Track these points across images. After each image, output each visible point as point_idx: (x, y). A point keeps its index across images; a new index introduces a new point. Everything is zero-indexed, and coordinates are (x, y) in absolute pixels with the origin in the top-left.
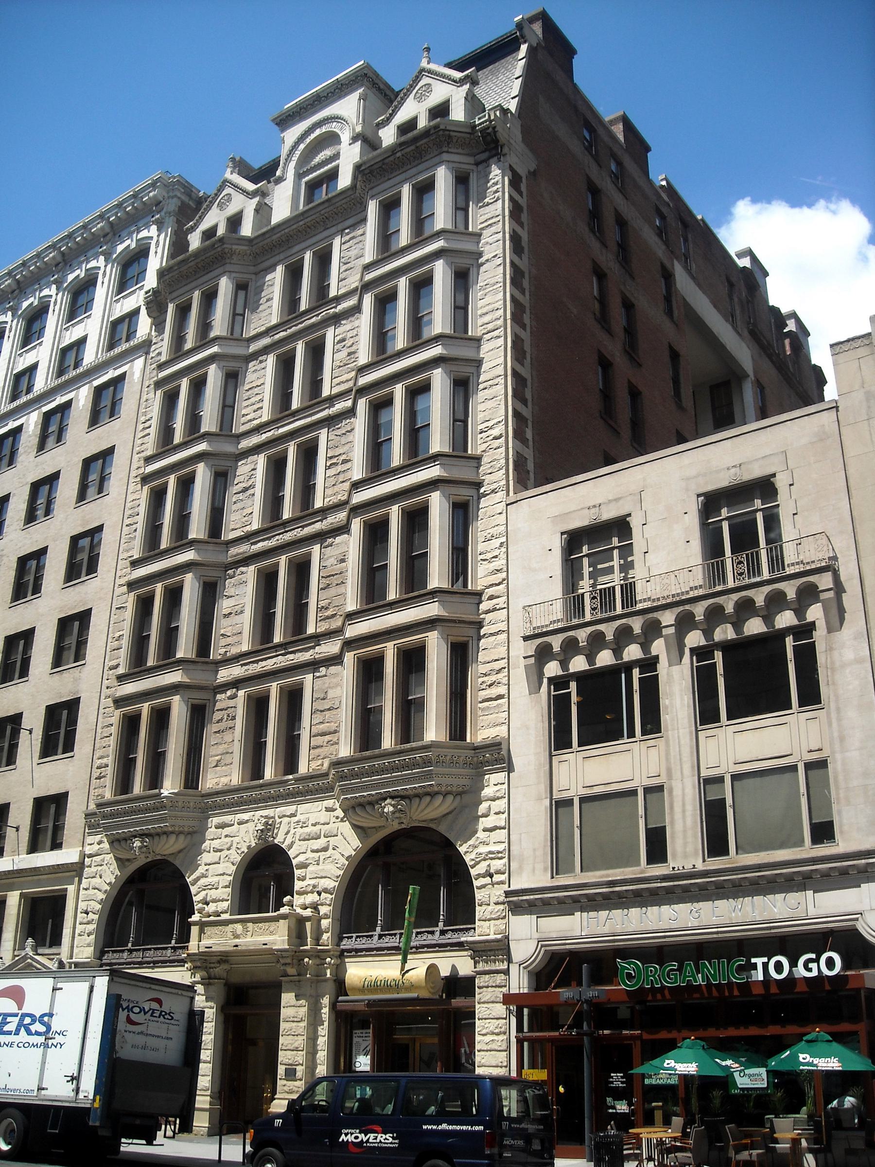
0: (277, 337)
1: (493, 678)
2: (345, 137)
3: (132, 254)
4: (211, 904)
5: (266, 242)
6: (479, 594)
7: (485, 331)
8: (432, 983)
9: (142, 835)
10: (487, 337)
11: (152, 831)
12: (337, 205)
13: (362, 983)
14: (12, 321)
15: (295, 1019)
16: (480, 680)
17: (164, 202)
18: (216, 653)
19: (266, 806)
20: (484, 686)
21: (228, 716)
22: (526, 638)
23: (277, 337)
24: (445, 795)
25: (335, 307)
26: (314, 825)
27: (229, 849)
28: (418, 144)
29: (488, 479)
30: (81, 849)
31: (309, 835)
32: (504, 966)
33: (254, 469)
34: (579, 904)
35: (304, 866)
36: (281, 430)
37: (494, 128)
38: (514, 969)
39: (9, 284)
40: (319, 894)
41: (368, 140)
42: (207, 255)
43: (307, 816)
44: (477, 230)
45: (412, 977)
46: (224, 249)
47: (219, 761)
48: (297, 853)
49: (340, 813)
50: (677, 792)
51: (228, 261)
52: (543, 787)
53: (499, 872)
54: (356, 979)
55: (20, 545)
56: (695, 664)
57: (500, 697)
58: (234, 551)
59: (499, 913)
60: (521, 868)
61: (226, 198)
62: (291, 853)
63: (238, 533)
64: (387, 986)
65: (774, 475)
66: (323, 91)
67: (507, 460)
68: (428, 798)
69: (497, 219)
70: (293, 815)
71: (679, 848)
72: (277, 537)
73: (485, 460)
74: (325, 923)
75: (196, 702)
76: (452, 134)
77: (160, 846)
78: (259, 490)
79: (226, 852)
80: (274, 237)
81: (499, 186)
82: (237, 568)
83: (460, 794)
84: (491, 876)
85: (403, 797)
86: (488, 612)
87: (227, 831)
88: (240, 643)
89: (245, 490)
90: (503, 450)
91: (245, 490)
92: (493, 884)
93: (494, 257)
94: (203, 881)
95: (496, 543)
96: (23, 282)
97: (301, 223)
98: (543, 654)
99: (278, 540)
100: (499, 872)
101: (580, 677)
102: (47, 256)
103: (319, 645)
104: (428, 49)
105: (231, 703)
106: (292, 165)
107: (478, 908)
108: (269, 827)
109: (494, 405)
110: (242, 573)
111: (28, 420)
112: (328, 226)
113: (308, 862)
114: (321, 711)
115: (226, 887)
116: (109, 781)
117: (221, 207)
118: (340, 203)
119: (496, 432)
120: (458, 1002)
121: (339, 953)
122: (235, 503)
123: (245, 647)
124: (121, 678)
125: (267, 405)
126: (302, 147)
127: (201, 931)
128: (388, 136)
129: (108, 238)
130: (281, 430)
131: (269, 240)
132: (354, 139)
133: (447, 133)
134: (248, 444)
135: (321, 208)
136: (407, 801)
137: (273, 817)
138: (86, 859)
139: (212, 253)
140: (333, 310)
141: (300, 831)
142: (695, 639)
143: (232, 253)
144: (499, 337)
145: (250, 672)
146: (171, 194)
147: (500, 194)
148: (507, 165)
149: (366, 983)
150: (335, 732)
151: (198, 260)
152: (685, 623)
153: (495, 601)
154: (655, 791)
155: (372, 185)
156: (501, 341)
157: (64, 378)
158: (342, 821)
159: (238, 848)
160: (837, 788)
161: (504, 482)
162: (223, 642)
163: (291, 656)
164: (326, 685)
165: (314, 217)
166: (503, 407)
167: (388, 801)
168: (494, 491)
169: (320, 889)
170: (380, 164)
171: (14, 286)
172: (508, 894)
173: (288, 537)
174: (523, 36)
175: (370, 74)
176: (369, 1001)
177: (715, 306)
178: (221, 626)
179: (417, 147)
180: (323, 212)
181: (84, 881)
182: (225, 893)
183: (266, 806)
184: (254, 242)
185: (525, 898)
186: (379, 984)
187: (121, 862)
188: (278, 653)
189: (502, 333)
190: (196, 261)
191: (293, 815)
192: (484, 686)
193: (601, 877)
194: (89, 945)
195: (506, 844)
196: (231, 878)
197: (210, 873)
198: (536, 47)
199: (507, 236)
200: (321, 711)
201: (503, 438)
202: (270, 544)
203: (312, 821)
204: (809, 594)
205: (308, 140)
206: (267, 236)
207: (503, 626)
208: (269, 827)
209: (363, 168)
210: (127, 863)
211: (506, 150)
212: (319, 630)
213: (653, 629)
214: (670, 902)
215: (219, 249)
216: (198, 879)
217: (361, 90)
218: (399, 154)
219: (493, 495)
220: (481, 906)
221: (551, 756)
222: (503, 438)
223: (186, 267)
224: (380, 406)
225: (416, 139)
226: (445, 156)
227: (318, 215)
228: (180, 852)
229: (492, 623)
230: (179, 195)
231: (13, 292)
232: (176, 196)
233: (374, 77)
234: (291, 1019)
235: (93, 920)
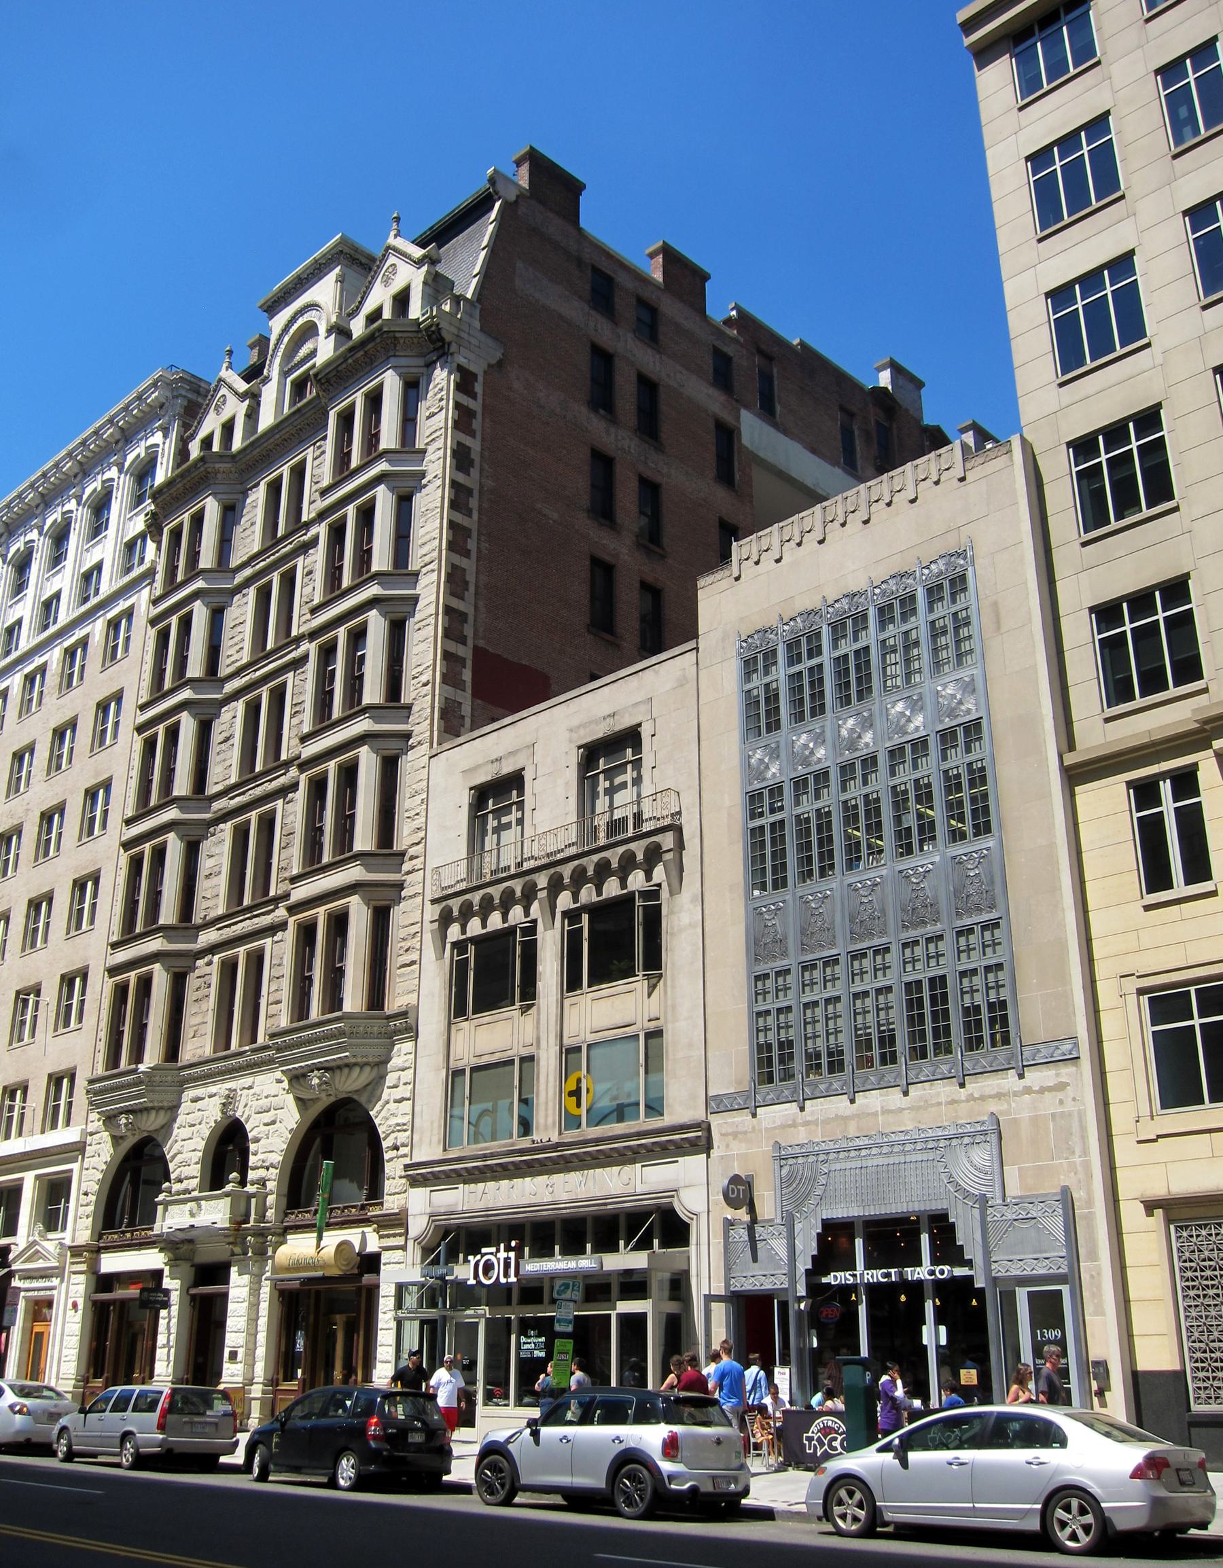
0: (258, 567)
2: (322, 329)
3: (144, 463)
6: (402, 854)
7: (422, 564)
8: (346, 1260)
9: (128, 1111)
10: (424, 570)
11: (135, 1107)
12: (307, 416)
14: (164, 443)
16: (399, 945)
17: (167, 404)
18: (197, 919)
22: (434, 901)
23: (258, 567)
25: (305, 534)
26: (266, 1097)
27: (200, 1124)
29: (417, 729)
30: (84, 1127)
32: (400, 1241)
33: (235, 717)
34: (462, 1178)
35: (257, 1140)
36: (258, 673)
37: (438, 325)
38: (410, 1244)
39: (156, 397)
41: (340, 331)
44: (422, 447)
48: (253, 1127)
49: (286, 1084)
50: (543, 1063)
52: (441, 1059)
53: (404, 1145)
55: (42, 798)
56: (566, 928)
57: (413, 963)
58: (218, 805)
61: (222, 400)
62: (248, 1127)
63: (219, 788)
65: (640, 725)
66: (303, 272)
67: (433, 708)
69: (438, 433)
70: (250, 1088)
71: (542, 1121)
72: (250, 792)
73: (415, 709)
74: (271, 1199)
75: (177, 970)
76: (398, 335)
77: (143, 1123)
78: (237, 741)
79: (198, 1127)
80: (255, 452)
81: (444, 393)
85: (327, 1069)
86: (409, 873)
87: (199, 1104)
88: (216, 906)
89: (227, 740)
90: (429, 697)
91: (227, 740)
93: (435, 477)
95: (418, 799)
96: (128, 429)
97: (277, 436)
98: (445, 919)
100: (404, 1145)
101: (475, 940)
102: (149, 396)
104: (398, 219)
105: (207, 970)
106: (277, 361)
107: (386, 1182)
108: (229, 1101)
109: (425, 648)
110: (222, 831)
111: (51, 657)
112: (304, 437)
113: (260, 1136)
114: (278, 978)
115: (197, 1163)
116: (101, 1058)
117: (386, 282)
118: (309, 414)
119: (424, 678)
120: (367, 1278)
121: (281, 1231)
122: (218, 754)
123: (221, 911)
124: (115, 946)
125: (247, 645)
126: (286, 339)
127: (166, 1210)
128: (358, 327)
129: (120, 445)
132: (329, 331)
133: (391, 334)
135: (293, 419)
136: (330, 1072)
137: (235, 1090)
138: (89, 1137)
141: (255, 1103)
142: (565, 900)
143: (217, 472)
144: (433, 571)
145: (224, 937)
146: (175, 394)
147: (443, 403)
148: (455, 365)
152: (556, 886)
153: (414, 862)
154: (528, 1060)
155: (331, 395)
156: (434, 576)
157: (88, 605)
158: (288, 1093)
160: (667, 1059)
161: (428, 733)
162: (205, 904)
163: (256, 920)
165: (287, 429)
166: (432, 649)
168: (420, 743)
169: (267, 1164)
170: (334, 373)
171: (118, 436)
172: (407, 1167)
173: (258, 792)
174: (497, 193)
175: (346, 250)
176: (304, 1278)
177: (814, 451)
178: (204, 887)
179: (366, 352)
180: (295, 424)
181: (86, 1160)
182: (195, 1170)
185: (419, 1172)
187: (116, 1140)
189: (436, 567)
191: (250, 1088)
195: (410, 1117)
196: (201, 1154)
197: (185, 1149)
198: (516, 202)
199: (449, 451)
200: (278, 978)
201: (430, 685)
204: (654, 855)
205: (292, 331)
206: (248, 451)
207: (419, 889)
208: (229, 1101)
210: (120, 1141)
211: (453, 348)
212: (279, 892)
213: (529, 895)
214: (532, 1175)
215: (202, 469)
216: (175, 1155)
217: (337, 270)
218: (350, 361)
219: (419, 748)
221: (450, 1024)
222: (430, 685)
223: (175, 489)
224: (328, 652)
225: (188, 470)
226: (393, 361)
228: (163, 1127)
229: (413, 884)
230: (184, 393)
231: (117, 442)
232: (180, 395)
233: (352, 252)
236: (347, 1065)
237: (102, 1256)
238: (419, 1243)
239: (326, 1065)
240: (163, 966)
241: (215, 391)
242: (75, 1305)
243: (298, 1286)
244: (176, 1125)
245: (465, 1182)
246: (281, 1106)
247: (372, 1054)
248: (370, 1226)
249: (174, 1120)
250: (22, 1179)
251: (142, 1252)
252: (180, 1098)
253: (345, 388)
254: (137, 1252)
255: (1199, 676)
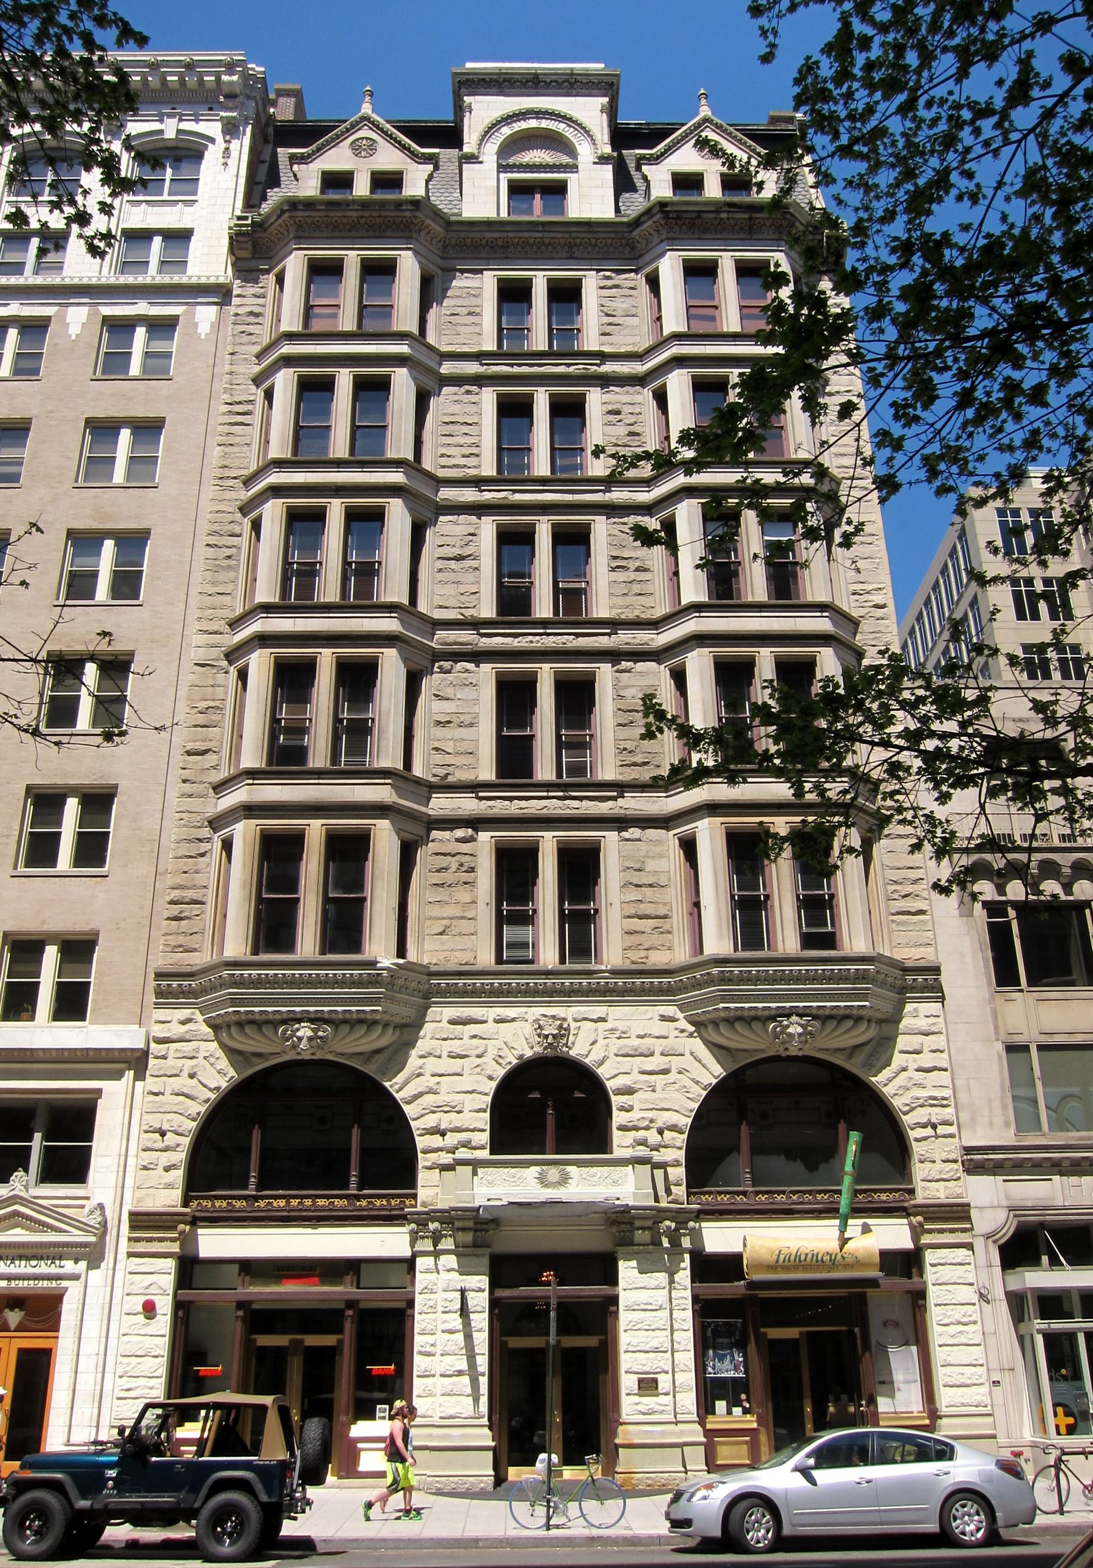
1: (910, 889)
4: (449, 1134)
5: (473, 235)
9: (316, 1020)
13: (775, 1257)
15: (650, 1307)
19: (550, 1002)
20: (896, 896)
21: (462, 865)
24: (386, 1025)
25: (598, 365)
28: (755, 215)
31: (636, 1050)
36: (518, 497)
40: (661, 1132)
42: (383, 213)
43: (628, 1023)
45: (857, 1250)
46: (415, 217)
47: (447, 927)
51: (415, 236)
54: (764, 1251)
59: (952, 1174)
60: (973, 1120)
64: (816, 1262)
68: (347, 1028)
72: (530, 638)
80: (488, 235)
82: (456, 662)
83: (880, 1022)
84: (163, 1134)
85: (815, 1017)
92: (937, 1137)
94: (428, 1100)
99: (531, 642)
103: (623, 797)
113: (637, 1086)
114: (637, 886)
130: (518, 497)
131: (478, 235)
134: (457, 496)
139: (393, 214)
140: (595, 368)
149: (782, 1257)
150: (665, 917)
151: (366, 214)
155: (672, 235)
159: (500, 1056)
164: (643, 853)
167: (794, 1018)
170: (693, 216)
180: (574, 235)
183: (550, 1002)
184: (454, 228)
186: (803, 1258)
188: (551, 794)
190: (361, 213)
191: (603, 1020)
192: (896, 896)
193: (1081, 1139)
194: (169, 1186)
202: (516, 644)
203: (636, 1032)
209: (668, 209)
210: (254, 1060)
215: (408, 214)
218: (724, 215)
220: (922, 1162)
227: (567, 235)
234: (642, 1307)
235: (178, 1145)
236: (374, 1023)
237: (200, 1231)
238: (995, 1242)
239: (814, 1012)
240: (393, 824)
241: (353, 126)
242: (149, 1309)
243: (743, 1291)
244: (414, 1053)
245: (1062, 1174)
246: (680, 1051)
247: (404, 1012)
248: (403, 1225)
249: (412, 1044)
250: (99, 1092)
251: (320, 1230)
252: (425, 1015)
253: (699, 239)
254: (309, 1230)
255: (101, 862)
